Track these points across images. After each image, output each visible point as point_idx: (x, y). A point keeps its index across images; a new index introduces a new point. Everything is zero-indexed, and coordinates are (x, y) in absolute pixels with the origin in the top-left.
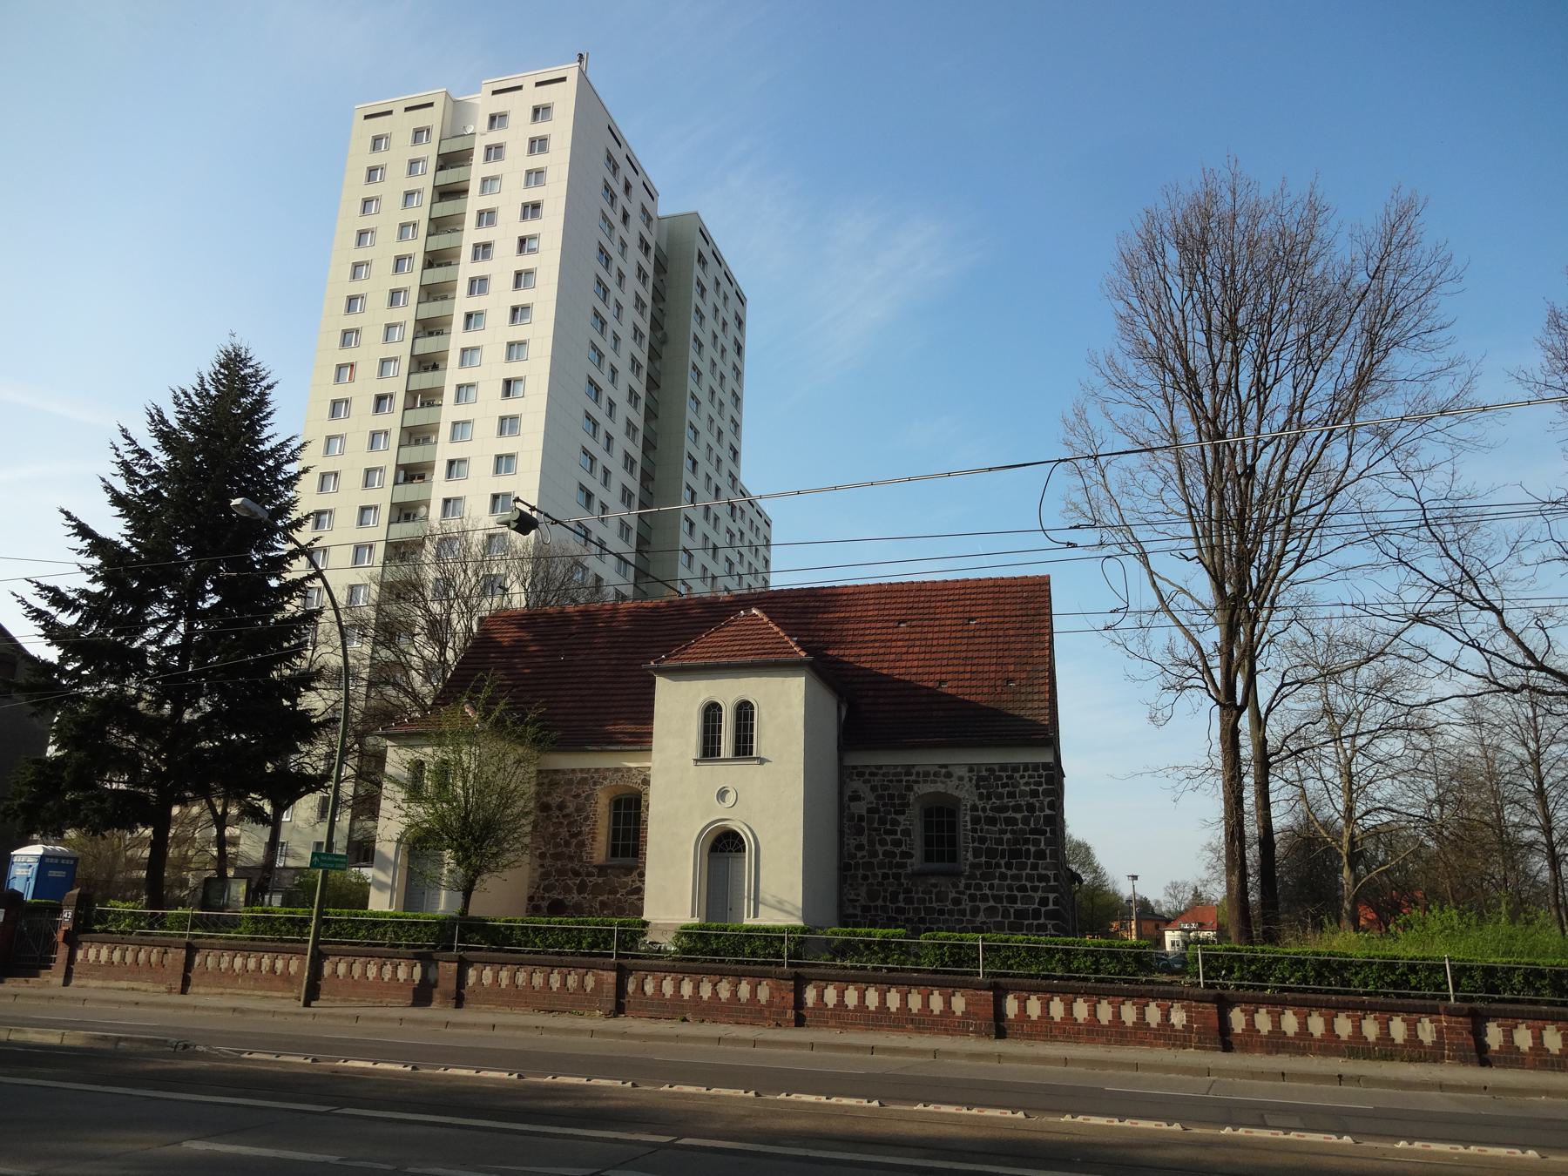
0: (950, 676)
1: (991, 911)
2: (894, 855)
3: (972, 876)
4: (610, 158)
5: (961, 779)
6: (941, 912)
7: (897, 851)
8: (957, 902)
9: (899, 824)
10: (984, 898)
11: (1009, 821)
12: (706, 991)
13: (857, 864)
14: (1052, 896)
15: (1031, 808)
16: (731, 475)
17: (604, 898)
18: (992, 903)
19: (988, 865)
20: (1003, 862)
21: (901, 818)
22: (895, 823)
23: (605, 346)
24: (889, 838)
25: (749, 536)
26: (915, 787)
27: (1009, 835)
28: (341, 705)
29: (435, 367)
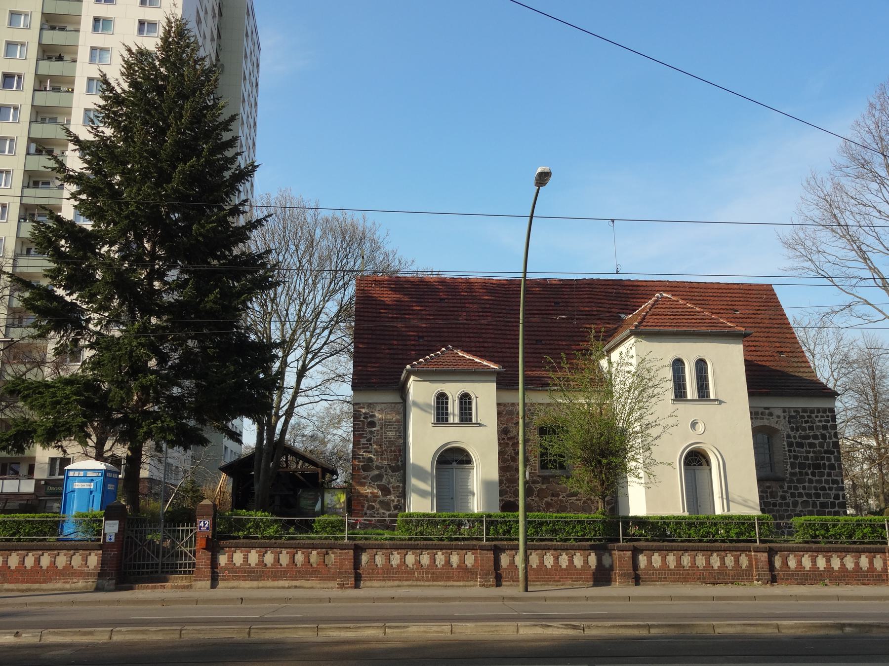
1: (805, 503)
3: (791, 481)
5: (779, 417)
6: (775, 505)
8: (784, 498)
10: (800, 495)
11: (811, 445)
12: (836, 563)
17: (549, 499)
18: (805, 498)
19: (801, 473)
20: (809, 472)
27: (811, 455)
29: (60, 58)
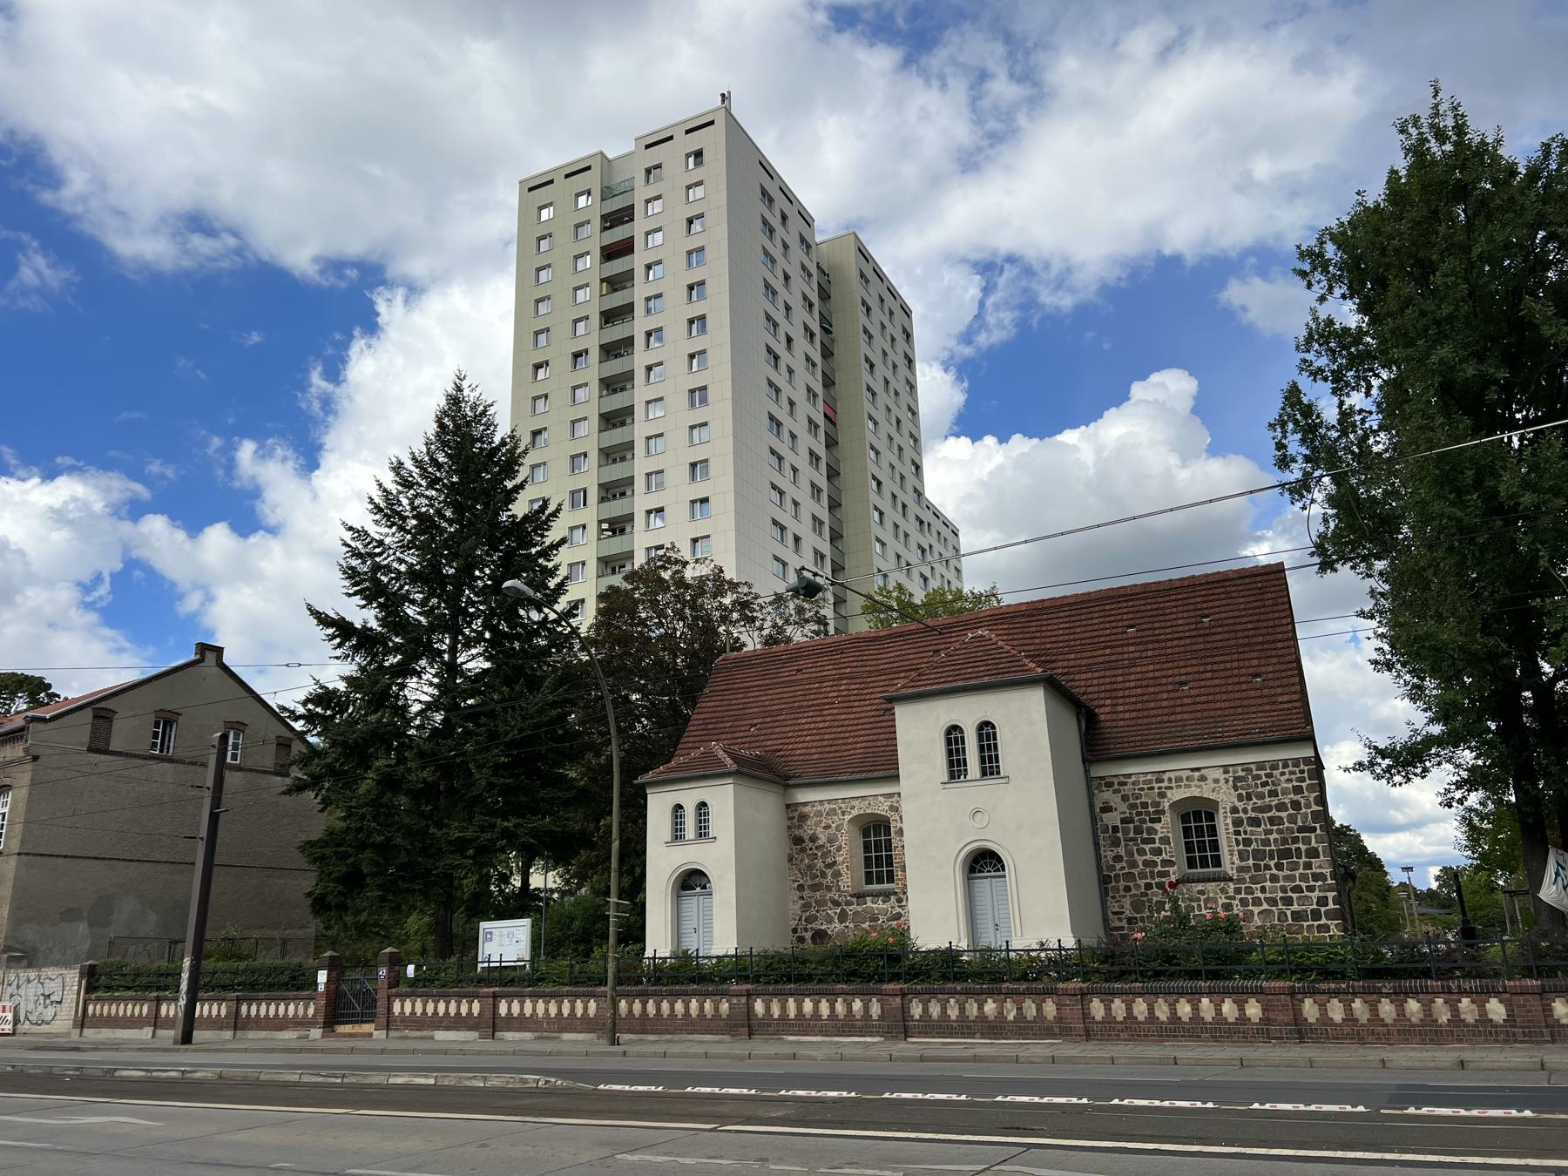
0: (1190, 677)
2: (1155, 864)
4: (764, 193)
5: (1216, 781)
7: (1158, 859)
9: (1156, 832)
10: (1257, 902)
13: (1117, 876)
14: (1331, 895)
15: (1296, 805)
16: (915, 490)
18: (1265, 906)
20: (1272, 863)
21: (1157, 826)
22: (1152, 831)
23: (781, 380)
24: (1147, 847)
25: (937, 547)
26: (1169, 793)
27: (1275, 835)
28: (1413, 814)
